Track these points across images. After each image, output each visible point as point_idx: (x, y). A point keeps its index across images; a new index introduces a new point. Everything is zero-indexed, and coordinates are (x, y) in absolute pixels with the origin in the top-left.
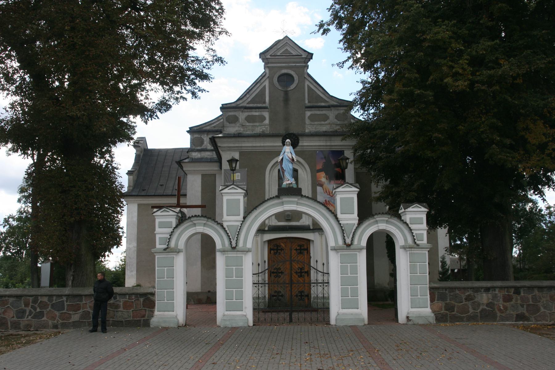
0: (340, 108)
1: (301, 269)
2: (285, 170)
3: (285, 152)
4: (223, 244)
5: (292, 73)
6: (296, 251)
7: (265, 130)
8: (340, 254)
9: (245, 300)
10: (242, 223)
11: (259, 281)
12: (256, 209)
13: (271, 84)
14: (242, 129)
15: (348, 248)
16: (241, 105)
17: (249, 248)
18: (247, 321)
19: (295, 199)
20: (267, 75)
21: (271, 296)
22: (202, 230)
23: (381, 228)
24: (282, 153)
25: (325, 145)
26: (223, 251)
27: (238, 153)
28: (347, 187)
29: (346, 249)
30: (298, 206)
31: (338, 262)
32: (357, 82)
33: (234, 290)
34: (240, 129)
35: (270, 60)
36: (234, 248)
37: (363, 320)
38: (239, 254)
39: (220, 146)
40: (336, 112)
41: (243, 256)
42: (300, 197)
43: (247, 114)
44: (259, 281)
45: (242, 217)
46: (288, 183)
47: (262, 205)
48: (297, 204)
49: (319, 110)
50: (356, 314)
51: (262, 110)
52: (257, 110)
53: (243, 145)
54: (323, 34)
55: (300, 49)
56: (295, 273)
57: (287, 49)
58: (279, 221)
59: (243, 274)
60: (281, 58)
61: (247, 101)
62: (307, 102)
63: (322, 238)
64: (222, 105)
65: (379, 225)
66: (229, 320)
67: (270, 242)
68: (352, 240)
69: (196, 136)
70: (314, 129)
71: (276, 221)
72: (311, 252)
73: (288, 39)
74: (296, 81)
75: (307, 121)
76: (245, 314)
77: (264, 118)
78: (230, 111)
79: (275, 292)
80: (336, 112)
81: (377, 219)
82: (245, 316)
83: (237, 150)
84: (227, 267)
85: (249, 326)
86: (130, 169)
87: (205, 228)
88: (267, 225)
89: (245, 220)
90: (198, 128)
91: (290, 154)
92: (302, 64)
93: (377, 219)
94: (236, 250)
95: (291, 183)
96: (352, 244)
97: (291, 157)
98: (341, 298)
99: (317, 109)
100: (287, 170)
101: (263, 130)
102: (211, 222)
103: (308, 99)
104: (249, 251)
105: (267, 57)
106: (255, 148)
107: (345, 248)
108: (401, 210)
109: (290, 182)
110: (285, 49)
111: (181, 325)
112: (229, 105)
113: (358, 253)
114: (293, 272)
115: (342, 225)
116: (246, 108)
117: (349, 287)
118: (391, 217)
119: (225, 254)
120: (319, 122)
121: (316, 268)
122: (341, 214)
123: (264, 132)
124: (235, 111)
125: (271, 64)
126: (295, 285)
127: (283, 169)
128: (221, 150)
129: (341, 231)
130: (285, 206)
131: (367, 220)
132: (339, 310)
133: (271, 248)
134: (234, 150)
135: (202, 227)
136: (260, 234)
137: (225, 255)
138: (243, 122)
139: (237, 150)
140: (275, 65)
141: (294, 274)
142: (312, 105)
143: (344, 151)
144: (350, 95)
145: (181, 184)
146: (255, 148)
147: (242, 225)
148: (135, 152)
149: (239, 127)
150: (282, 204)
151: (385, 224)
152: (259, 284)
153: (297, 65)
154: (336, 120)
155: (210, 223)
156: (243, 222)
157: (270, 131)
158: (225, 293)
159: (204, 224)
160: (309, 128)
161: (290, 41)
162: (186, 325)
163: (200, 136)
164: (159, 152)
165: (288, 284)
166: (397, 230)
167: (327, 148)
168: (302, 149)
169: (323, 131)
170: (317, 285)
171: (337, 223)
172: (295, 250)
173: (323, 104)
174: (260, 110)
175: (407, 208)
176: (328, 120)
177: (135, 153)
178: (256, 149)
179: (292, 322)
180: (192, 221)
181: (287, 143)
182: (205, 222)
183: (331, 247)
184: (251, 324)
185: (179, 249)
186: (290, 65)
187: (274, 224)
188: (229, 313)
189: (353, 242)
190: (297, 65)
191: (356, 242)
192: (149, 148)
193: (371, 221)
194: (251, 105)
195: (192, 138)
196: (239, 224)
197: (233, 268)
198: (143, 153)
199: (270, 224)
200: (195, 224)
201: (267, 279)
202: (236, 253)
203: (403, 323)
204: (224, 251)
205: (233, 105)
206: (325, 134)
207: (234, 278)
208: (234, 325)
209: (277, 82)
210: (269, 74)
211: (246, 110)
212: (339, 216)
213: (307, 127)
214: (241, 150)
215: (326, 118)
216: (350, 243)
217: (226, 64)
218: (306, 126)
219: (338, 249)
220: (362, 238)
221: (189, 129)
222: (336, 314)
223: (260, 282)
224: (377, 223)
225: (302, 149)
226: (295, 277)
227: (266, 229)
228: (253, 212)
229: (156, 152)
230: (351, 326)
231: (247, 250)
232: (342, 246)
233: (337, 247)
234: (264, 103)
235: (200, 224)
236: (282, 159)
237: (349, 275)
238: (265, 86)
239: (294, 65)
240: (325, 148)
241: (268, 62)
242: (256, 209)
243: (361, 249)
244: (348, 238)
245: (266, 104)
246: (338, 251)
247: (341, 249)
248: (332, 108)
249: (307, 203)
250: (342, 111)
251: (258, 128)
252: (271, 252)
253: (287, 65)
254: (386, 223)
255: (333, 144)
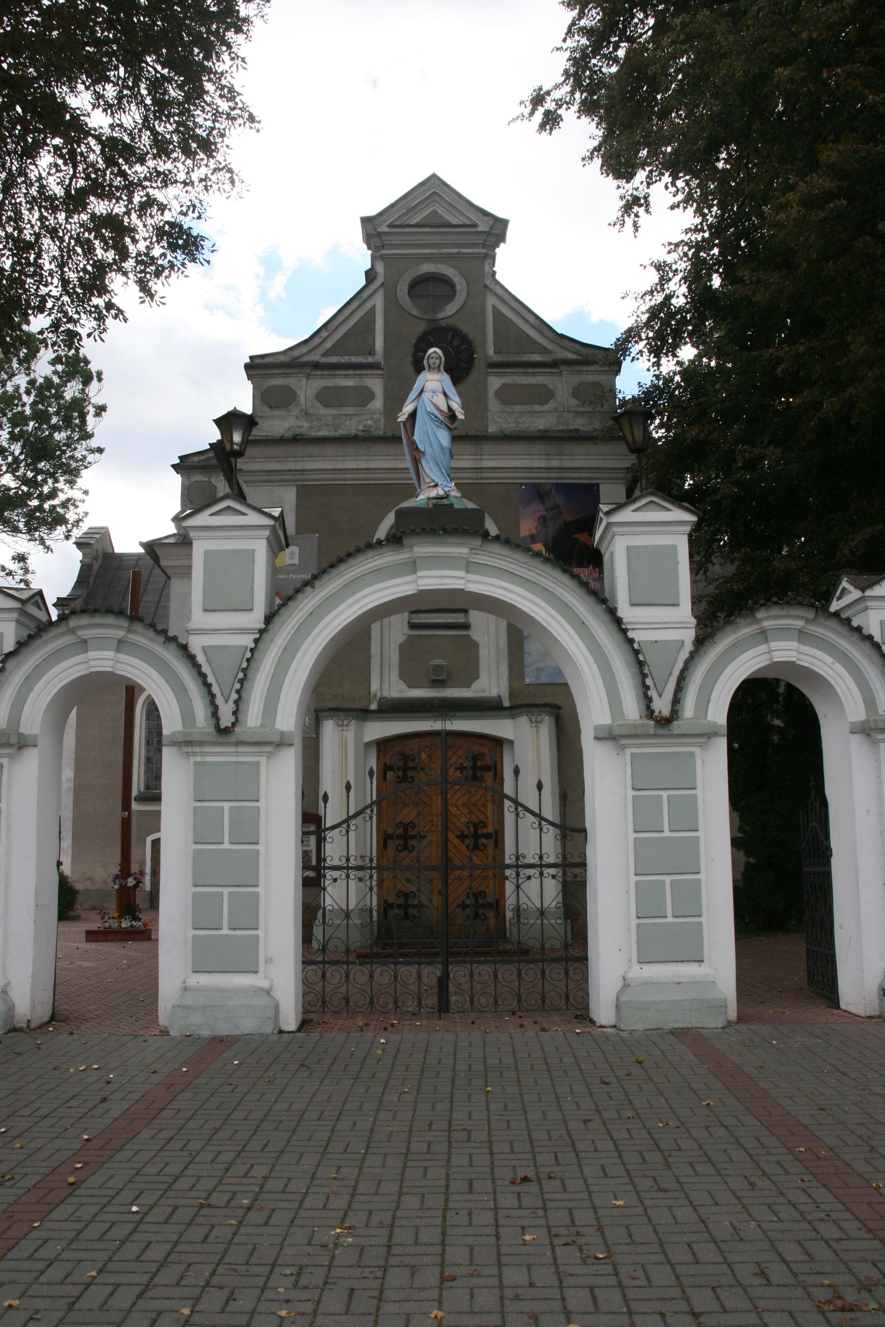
0: (584, 368)
1: (476, 826)
2: (423, 453)
3: (422, 391)
4: (187, 716)
5: (450, 272)
6: (461, 773)
7: (370, 426)
8: (632, 754)
9: (266, 931)
10: (257, 636)
11: (348, 860)
12: (313, 587)
13: (391, 301)
14: (305, 424)
15: (661, 731)
16: (305, 359)
17: (282, 733)
18: (272, 1014)
19: (459, 549)
20: (380, 279)
21: (385, 907)
22: (111, 663)
23: (778, 657)
24: (413, 395)
25: (544, 465)
26: (186, 743)
27: (295, 489)
28: (651, 506)
29: (656, 736)
30: (471, 577)
31: (625, 785)
32: (641, 265)
33: (226, 891)
34: (300, 424)
35: (389, 238)
36: (224, 732)
37: (724, 1006)
38: (246, 756)
39: (240, 470)
40: (575, 380)
41: (263, 760)
42: (478, 542)
43: (318, 384)
44: (348, 860)
45: (262, 619)
46: (433, 493)
47: (334, 572)
48: (469, 567)
49: (527, 374)
50: (697, 984)
51: (364, 372)
52: (351, 372)
53: (309, 465)
54: (542, 127)
55: (471, 208)
56: (457, 837)
57: (435, 212)
58: (410, 686)
59: (262, 830)
60: (417, 233)
61: (322, 349)
62: (491, 351)
63: (537, 731)
64: (251, 358)
65: (774, 645)
66: (204, 1007)
67: (383, 744)
68: (676, 700)
69: (198, 478)
70: (511, 425)
71: (403, 685)
72: (505, 777)
73: (437, 182)
74: (461, 295)
75: (493, 404)
76: (265, 984)
77: (370, 396)
78: (273, 376)
79: (399, 894)
80: (575, 380)
81: (765, 624)
82: (268, 992)
83: (291, 481)
84: (198, 804)
85: (281, 1032)
86: (64, 594)
87: (122, 657)
88: (375, 696)
89: (270, 627)
90: (203, 458)
91: (442, 397)
92: (476, 251)
93: (765, 624)
94: (232, 739)
95: (447, 496)
96: (675, 714)
97: (444, 408)
98: (634, 922)
99: (521, 370)
100: (428, 451)
101: (365, 426)
102: (143, 635)
103: (494, 344)
104: (282, 743)
105: (379, 230)
106: (342, 476)
107: (652, 731)
108: (839, 598)
109: (441, 493)
110: (431, 210)
111: (24, 1025)
112: (270, 360)
113: (697, 750)
114: (451, 836)
115: (636, 646)
116: (317, 366)
117: (668, 879)
118: (816, 618)
119: (194, 754)
120: (525, 407)
121: (537, 811)
122: (632, 605)
123: (369, 431)
124: (288, 375)
125: (391, 249)
126: (457, 872)
127: (417, 448)
128: (246, 482)
129: (635, 668)
130: (419, 574)
131: (729, 629)
132: (630, 968)
133: (385, 763)
134: (282, 481)
135: (111, 654)
136: (353, 721)
137: (192, 759)
138: (309, 404)
139: (291, 481)
140: (403, 251)
141: (456, 841)
142: (505, 359)
143: (598, 485)
144: (623, 298)
145: (142, 589)
146: (342, 476)
147: (261, 645)
148: (81, 558)
149: (297, 417)
150: (412, 566)
151: (794, 644)
152: (348, 868)
153: (464, 251)
154: (574, 402)
155: (142, 638)
156: (262, 632)
157: (385, 427)
158: (190, 903)
159: (120, 642)
160: (499, 420)
161: (444, 187)
162: (53, 1018)
163: (206, 479)
164: (138, 560)
165: (432, 868)
166: (838, 667)
167: (549, 475)
168: (477, 479)
169: (539, 431)
170: (541, 874)
171: (619, 637)
172: (456, 769)
173: (537, 358)
174: (358, 372)
175: (871, 586)
176: (551, 401)
177: (81, 561)
178: (345, 480)
179: (448, 1011)
180: (73, 631)
181: (431, 361)
182: (120, 634)
183: (596, 728)
184: (290, 1020)
185: (20, 735)
186: (444, 251)
187: (395, 694)
188: (203, 980)
189: (678, 707)
190: (464, 251)
191: (688, 709)
192: (116, 551)
193: (744, 630)
194: (334, 359)
195: (186, 483)
196: (248, 641)
197: (223, 808)
198: (100, 562)
199: (386, 694)
200: (85, 642)
201: (509, 887)
202: (233, 749)
203: (868, 1014)
204: (190, 743)
205: (283, 358)
206: (544, 434)
207: (226, 846)
208: (223, 1029)
209: (407, 297)
210: (385, 277)
211: (319, 373)
212: (625, 611)
213: (493, 419)
214: (302, 480)
215: (545, 395)
216: (666, 713)
217: (244, 194)
218: (490, 417)
219: (623, 736)
220: (712, 698)
221: (178, 461)
222: (618, 985)
223: (353, 863)
224: (767, 641)
225: (477, 479)
226: (459, 850)
227: (374, 706)
228: (300, 596)
229: (131, 560)
230: (679, 1033)
231: (276, 739)
232: (641, 722)
233: (620, 726)
234: (370, 354)
235: (102, 643)
236: (413, 415)
237: (667, 834)
238: (374, 308)
239: (455, 251)
240: (544, 475)
241: (383, 246)
242: (313, 587)
243: (710, 735)
244: (660, 695)
245: (376, 357)
246: (624, 742)
247: (636, 736)
248: (563, 368)
249: (503, 564)
250: (591, 375)
251: (351, 419)
252: (388, 776)
253: (435, 251)
254: (800, 642)
255: (567, 464)
